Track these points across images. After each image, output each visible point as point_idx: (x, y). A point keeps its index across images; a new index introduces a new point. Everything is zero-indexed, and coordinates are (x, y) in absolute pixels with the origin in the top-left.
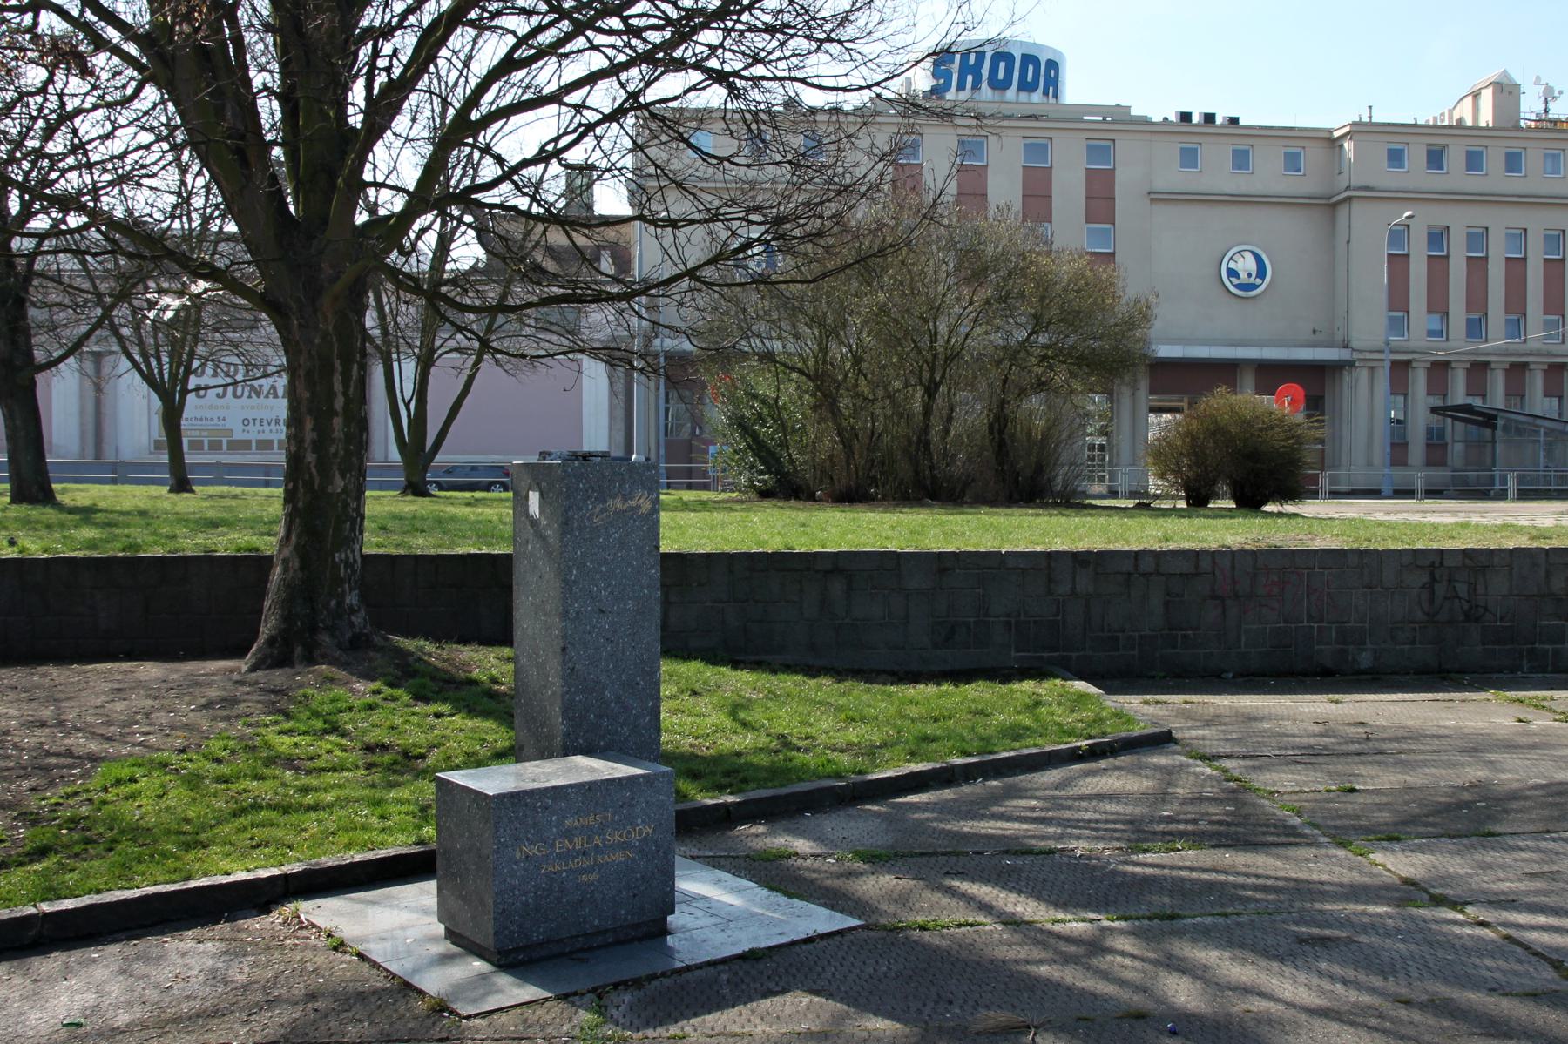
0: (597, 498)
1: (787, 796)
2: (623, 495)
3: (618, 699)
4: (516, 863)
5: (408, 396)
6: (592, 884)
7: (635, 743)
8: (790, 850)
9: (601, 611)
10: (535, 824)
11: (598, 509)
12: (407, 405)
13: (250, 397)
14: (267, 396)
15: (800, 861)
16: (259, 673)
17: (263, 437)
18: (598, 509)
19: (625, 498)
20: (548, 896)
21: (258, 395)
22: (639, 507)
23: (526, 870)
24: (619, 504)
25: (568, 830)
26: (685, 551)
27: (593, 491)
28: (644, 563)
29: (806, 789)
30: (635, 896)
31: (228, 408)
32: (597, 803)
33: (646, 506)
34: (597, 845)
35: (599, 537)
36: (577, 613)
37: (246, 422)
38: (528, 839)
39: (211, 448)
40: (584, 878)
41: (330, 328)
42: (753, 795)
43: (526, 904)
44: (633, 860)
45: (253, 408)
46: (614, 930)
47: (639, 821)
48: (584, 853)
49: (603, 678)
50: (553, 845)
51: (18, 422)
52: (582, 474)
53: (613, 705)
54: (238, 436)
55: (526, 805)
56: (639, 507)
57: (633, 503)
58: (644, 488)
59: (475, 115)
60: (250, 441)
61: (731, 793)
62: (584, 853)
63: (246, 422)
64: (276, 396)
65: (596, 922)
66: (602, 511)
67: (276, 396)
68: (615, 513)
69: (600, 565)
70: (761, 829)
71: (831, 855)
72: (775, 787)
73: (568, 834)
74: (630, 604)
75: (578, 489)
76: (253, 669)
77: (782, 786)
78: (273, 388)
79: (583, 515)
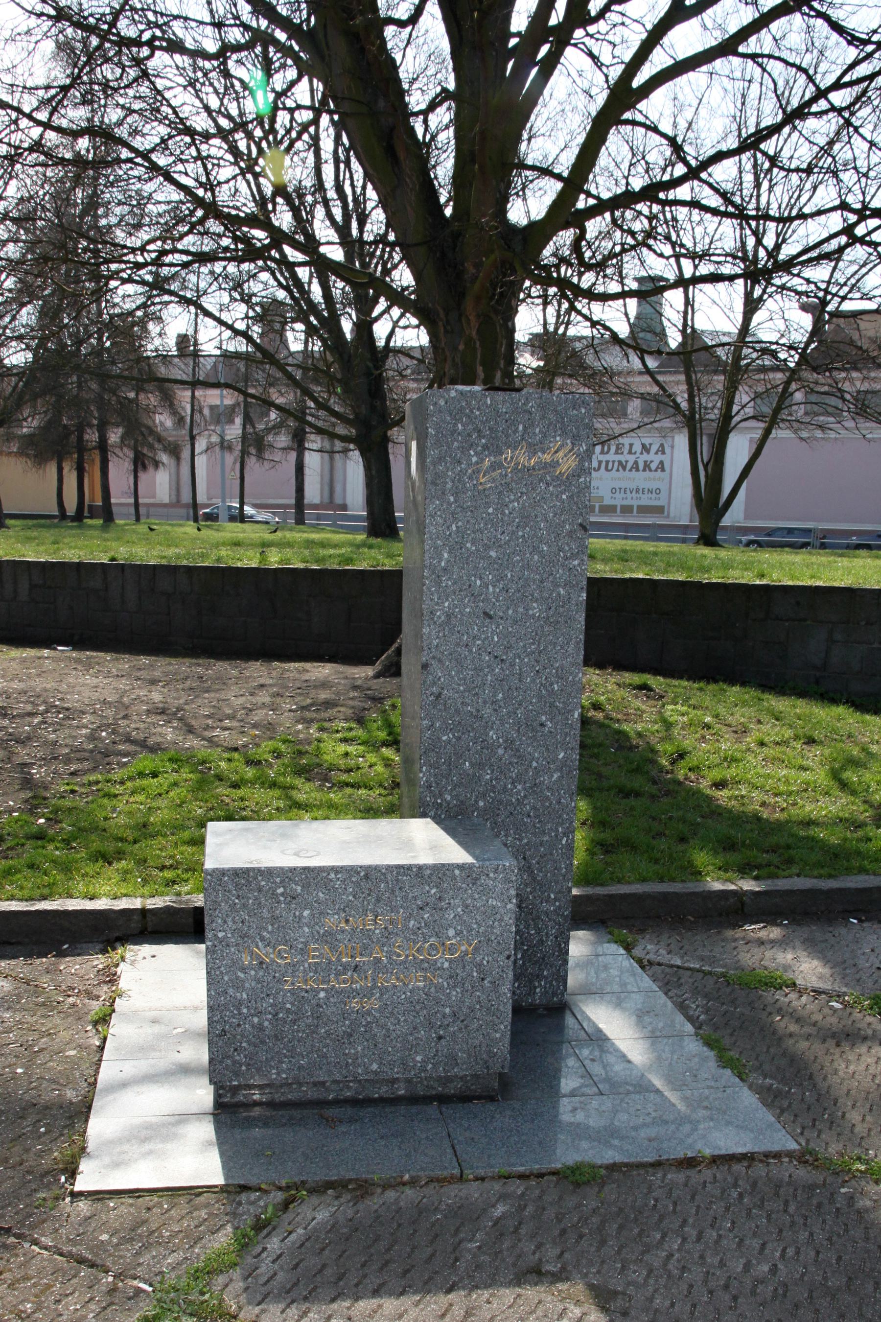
0: (485, 447)
1: (831, 892)
2: (530, 445)
3: (509, 744)
4: (243, 969)
5: (705, 459)
6: (369, 1013)
7: (534, 808)
8: (789, 975)
9: (487, 615)
10: (274, 919)
11: (487, 463)
12: (706, 467)
13: (618, 470)
14: (630, 470)
15: (793, 996)
16: (381, 680)
17: (625, 503)
18: (487, 463)
19: (533, 450)
20: (294, 1022)
21: (624, 468)
22: (555, 464)
23: (258, 981)
24: (523, 458)
25: (329, 933)
26: (855, 586)
27: (480, 437)
28: (560, 550)
29: (860, 885)
30: (440, 1038)
31: (601, 479)
32: (378, 900)
33: (567, 464)
34: (378, 960)
35: (488, 505)
36: (449, 616)
37: (613, 491)
38: (262, 939)
39: (600, 511)
40: (355, 1004)
41: (474, 333)
42: (782, 884)
43: (260, 1028)
44: (439, 988)
45: (619, 479)
46: (409, 1081)
47: (451, 932)
48: (356, 968)
49: (487, 711)
50: (303, 951)
51: (374, 472)
52: (462, 409)
53: (501, 751)
54: (607, 501)
55: (260, 890)
56: (555, 464)
57: (547, 457)
58: (564, 434)
59: (636, 83)
60: (632, 506)
61: (756, 878)
62: (356, 968)
63: (613, 491)
64: (637, 470)
65: (375, 1066)
66: (493, 467)
67: (637, 470)
68: (515, 469)
69: (487, 548)
70: (775, 933)
71: (839, 996)
72: (820, 877)
73: (328, 938)
74: (536, 609)
75: (454, 432)
76: (377, 676)
77: (830, 876)
78: (636, 463)
79: (462, 472)
